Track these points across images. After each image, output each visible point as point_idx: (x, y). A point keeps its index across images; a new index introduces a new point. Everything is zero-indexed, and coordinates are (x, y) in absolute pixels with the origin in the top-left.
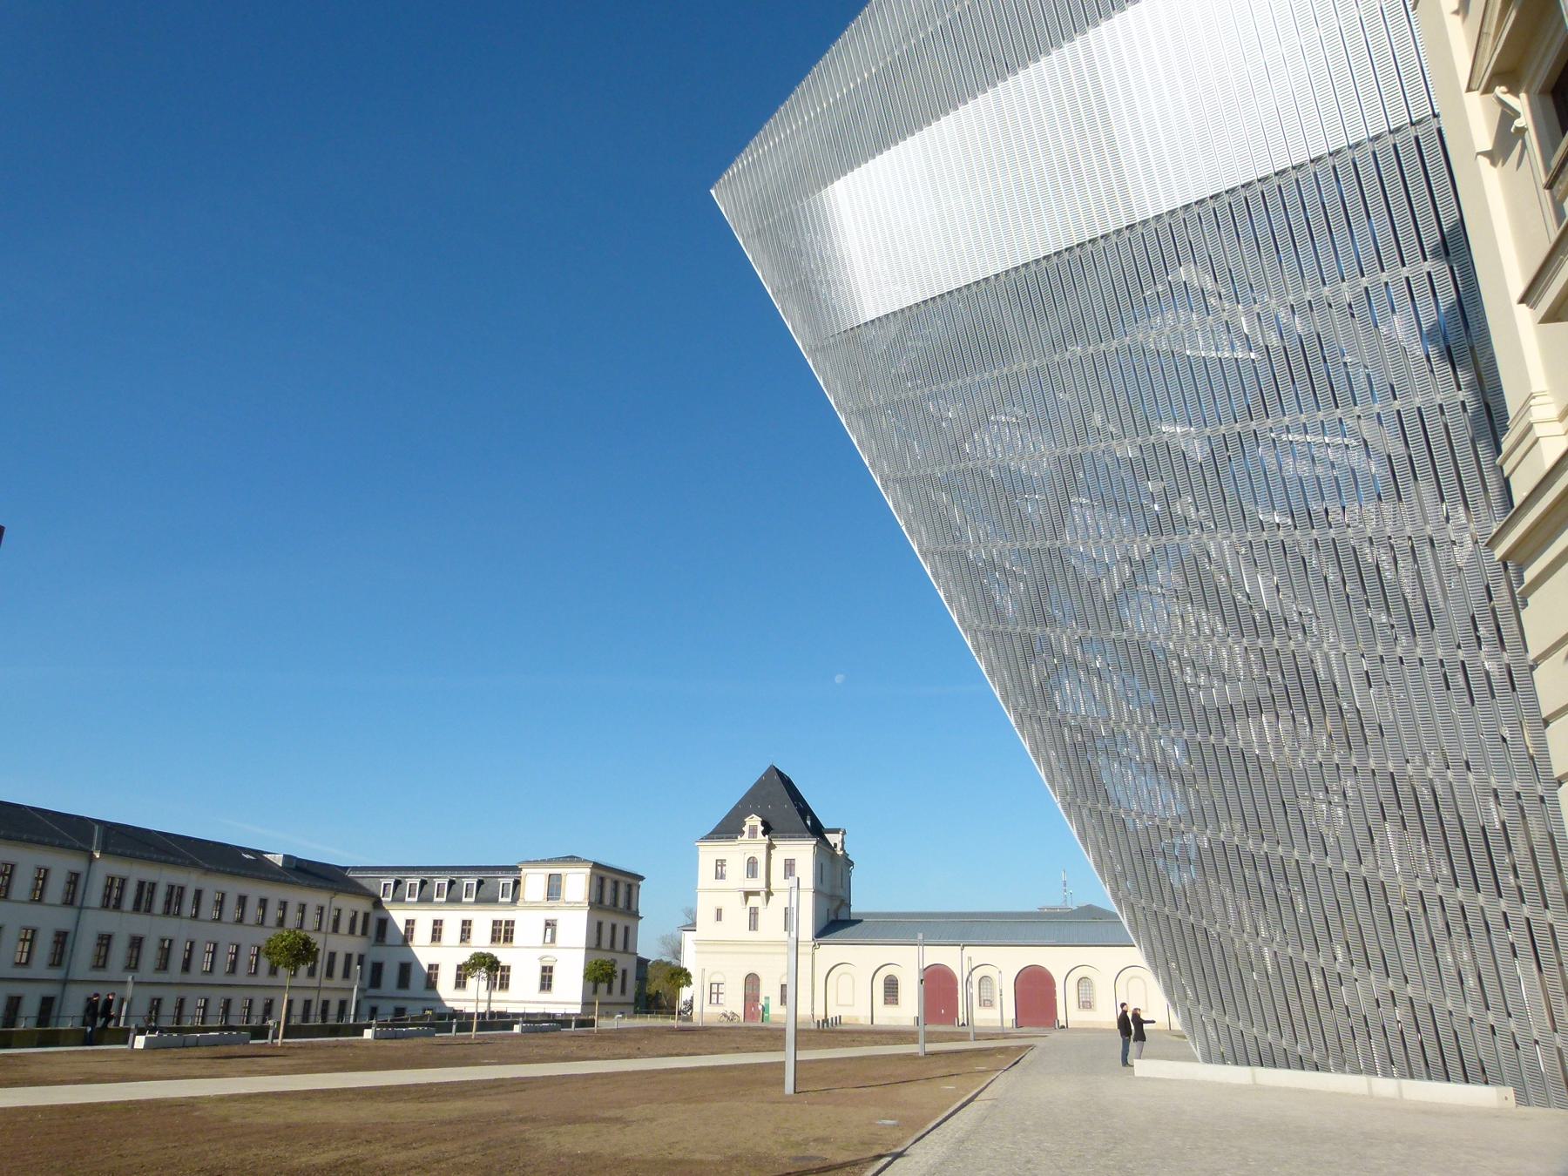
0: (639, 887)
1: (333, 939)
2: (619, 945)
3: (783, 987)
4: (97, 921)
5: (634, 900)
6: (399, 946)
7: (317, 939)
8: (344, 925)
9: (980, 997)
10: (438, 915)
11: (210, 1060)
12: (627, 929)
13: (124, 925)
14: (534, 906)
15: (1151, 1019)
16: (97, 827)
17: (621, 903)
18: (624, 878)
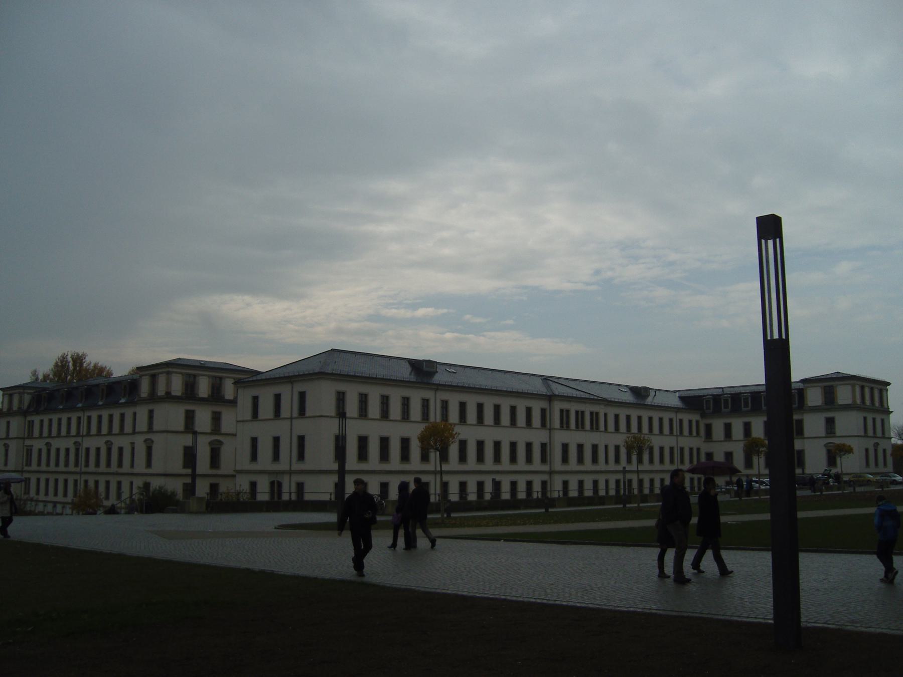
0: (887, 390)
1: (680, 439)
2: (879, 433)
3: (867, 450)
4: (561, 437)
6: (721, 441)
7: (463, 432)
10: (727, 421)
12: (883, 421)
13: (573, 438)
14: (815, 409)
15: (153, 462)
16: (424, 363)
18: (868, 384)
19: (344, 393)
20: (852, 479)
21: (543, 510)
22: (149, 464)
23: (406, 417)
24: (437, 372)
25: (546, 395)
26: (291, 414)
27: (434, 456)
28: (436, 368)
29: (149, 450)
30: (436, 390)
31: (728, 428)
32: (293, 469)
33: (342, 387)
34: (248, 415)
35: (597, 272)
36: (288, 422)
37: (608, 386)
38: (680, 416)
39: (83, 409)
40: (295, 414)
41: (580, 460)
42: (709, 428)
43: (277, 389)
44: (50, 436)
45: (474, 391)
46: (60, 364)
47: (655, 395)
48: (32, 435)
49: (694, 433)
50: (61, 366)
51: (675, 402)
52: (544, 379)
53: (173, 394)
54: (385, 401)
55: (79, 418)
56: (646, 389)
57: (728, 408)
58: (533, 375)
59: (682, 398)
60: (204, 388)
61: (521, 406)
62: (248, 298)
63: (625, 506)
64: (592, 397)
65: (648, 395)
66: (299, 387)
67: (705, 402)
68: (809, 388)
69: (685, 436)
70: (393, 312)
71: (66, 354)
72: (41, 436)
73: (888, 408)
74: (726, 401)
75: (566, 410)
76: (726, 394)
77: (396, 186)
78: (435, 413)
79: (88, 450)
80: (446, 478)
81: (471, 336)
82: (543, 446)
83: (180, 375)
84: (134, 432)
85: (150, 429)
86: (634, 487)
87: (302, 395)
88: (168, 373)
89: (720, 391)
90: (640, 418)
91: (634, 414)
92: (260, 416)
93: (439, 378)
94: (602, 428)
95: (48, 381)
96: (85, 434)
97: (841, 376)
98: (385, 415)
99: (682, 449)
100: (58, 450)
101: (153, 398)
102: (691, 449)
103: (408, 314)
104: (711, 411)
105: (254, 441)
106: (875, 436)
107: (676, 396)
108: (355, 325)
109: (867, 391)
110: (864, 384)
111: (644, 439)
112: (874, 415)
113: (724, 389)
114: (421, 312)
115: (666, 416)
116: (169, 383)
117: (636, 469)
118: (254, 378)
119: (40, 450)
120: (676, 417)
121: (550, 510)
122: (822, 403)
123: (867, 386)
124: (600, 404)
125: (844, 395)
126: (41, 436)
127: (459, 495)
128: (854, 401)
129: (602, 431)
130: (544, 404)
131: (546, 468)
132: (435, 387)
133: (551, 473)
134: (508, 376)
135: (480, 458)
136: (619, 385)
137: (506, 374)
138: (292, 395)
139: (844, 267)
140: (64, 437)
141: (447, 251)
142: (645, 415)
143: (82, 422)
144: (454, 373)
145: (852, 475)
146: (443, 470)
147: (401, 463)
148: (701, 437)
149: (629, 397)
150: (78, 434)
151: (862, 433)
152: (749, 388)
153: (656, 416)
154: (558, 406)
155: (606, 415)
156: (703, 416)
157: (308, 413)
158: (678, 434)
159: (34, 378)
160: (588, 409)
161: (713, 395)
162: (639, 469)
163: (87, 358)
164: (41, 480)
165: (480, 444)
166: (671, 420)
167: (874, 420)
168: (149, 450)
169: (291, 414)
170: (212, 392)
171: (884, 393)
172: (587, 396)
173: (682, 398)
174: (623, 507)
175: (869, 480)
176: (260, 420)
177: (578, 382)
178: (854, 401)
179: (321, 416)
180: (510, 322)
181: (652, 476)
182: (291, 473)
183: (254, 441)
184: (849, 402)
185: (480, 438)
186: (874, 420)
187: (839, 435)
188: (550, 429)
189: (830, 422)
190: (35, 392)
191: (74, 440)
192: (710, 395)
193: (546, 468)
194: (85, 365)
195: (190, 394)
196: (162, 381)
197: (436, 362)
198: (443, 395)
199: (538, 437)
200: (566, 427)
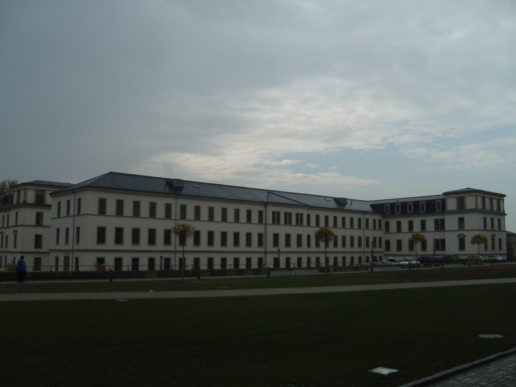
0: (503, 200)
4: (272, 229)
5: (501, 207)
7: (335, 231)
8: (371, 226)
9: (74, 225)
10: (399, 220)
13: (282, 230)
14: (452, 212)
16: (175, 181)
17: (495, 209)
18: (495, 197)
19: (122, 201)
24: (184, 187)
25: (263, 202)
26: (74, 214)
27: (322, 244)
31: (399, 224)
33: (103, 195)
35: (385, 139)
37: (295, 195)
38: (366, 217)
40: (76, 214)
41: (352, 245)
42: (387, 224)
45: (198, 198)
47: (352, 203)
49: (377, 228)
52: (268, 192)
53: (28, 202)
56: (345, 200)
59: (372, 206)
63: (111, 281)
65: (346, 204)
66: (79, 196)
67: (385, 208)
70: (267, 162)
73: (504, 212)
74: (398, 207)
77: (274, 93)
78: (176, 213)
80: (328, 255)
81: (310, 175)
82: (260, 236)
83: (33, 190)
87: (79, 200)
89: (396, 201)
90: (352, 219)
92: (61, 216)
98: (224, 219)
99: (368, 238)
101: (19, 205)
109: (487, 201)
112: (492, 216)
113: (398, 200)
114: (285, 162)
116: (25, 195)
117: (324, 250)
118: (67, 189)
121: (114, 280)
122: (457, 208)
124: (303, 208)
125: (470, 203)
127: (148, 266)
129: (305, 226)
130: (262, 208)
131: (262, 249)
133: (265, 253)
138: (75, 201)
141: (300, 128)
144: (198, 187)
145: (469, 256)
146: (184, 250)
147: (208, 247)
148: (383, 230)
149: (333, 205)
151: (483, 228)
153: (348, 217)
154: (271, 209)
156: (384, 216)
157: (82, 213)
160: (294, 212)
162: (327, 251)
164: (3, 257)
166: (359, 220)
167: (492, 219)
169: (74, 214)
171: (501, 202)
172: (294, 203)
173: (372, 206)
176: (311, 227)
179: (87, 214)
180: (335, 167)
183: (58, 230)
186: (492, 219)
187: (143, 216)
189: (461, 220)
192: (389, 203)
193: (276, 249)
196: (22, 193)
199: (255, 229)
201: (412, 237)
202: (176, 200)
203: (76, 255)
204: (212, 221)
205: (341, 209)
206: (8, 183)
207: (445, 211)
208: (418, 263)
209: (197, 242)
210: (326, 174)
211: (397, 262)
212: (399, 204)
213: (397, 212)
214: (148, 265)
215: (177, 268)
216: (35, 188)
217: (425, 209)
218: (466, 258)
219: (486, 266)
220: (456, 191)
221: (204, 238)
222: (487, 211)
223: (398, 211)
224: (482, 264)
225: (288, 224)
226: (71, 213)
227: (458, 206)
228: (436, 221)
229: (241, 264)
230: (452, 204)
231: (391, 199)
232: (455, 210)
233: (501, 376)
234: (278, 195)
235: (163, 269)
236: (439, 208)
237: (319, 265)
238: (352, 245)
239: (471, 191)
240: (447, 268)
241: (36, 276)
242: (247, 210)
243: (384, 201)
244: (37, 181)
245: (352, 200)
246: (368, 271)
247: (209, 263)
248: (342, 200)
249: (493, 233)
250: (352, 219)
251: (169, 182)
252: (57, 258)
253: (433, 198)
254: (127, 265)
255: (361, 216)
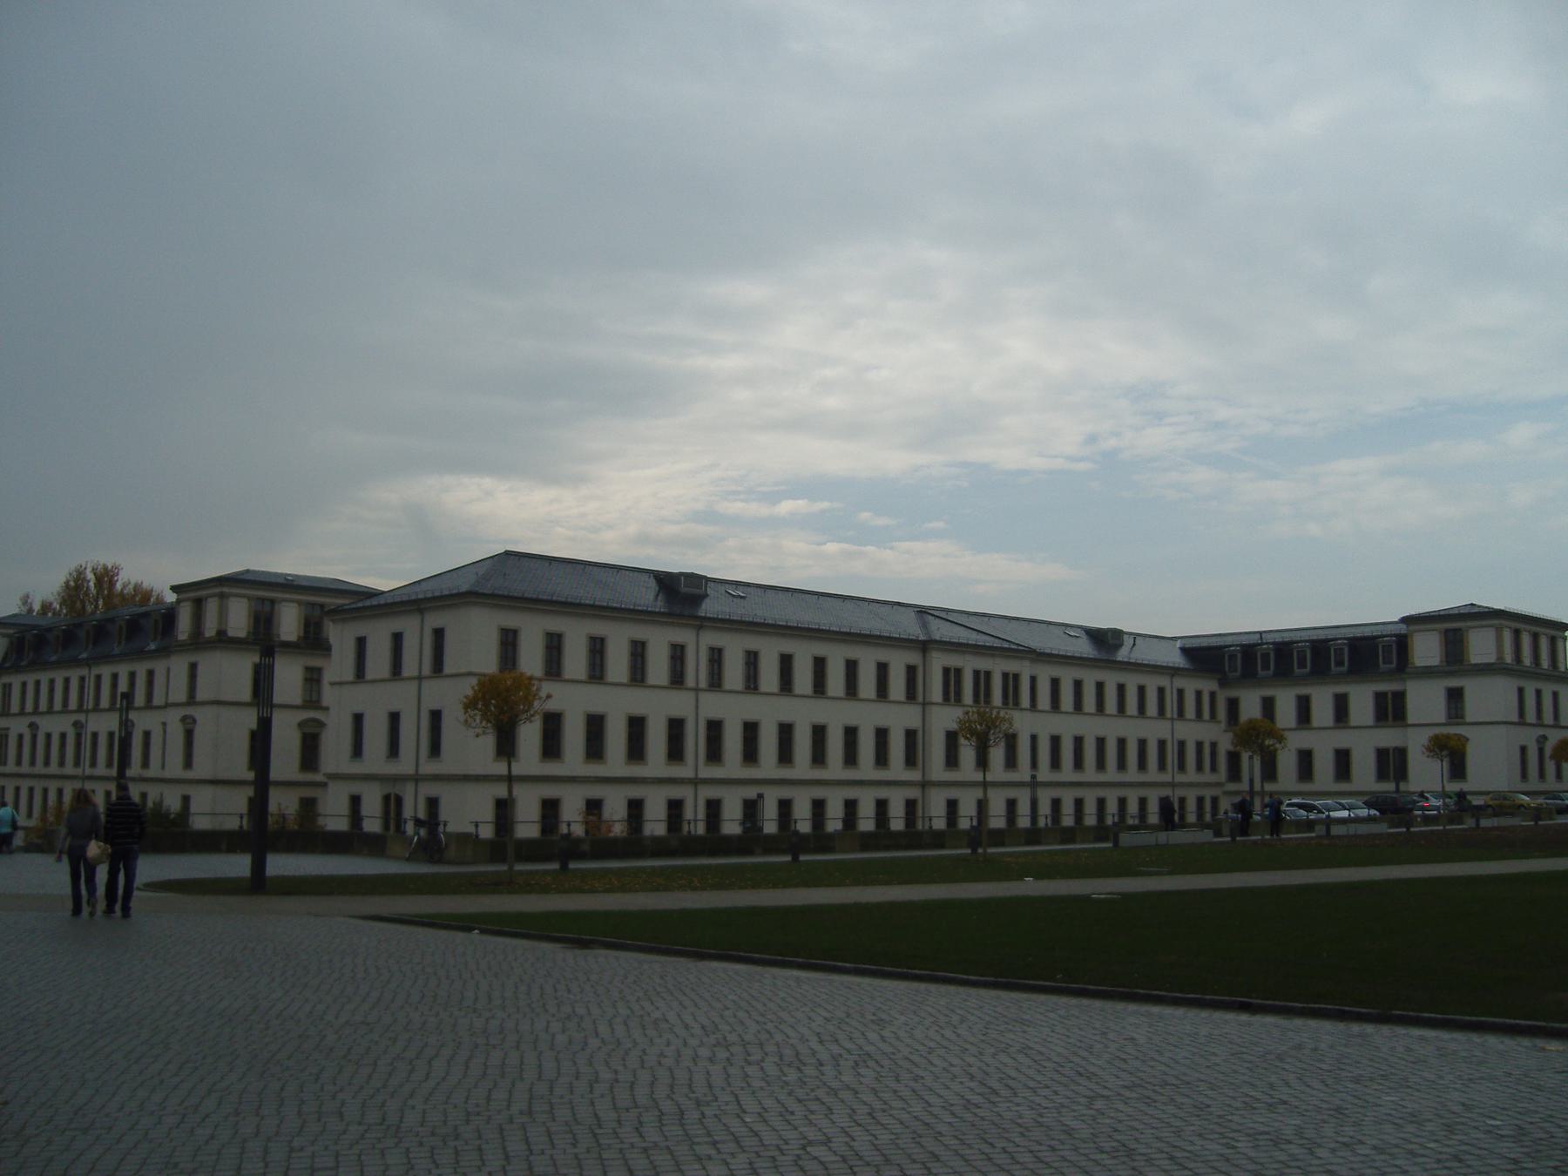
1: (1179, 725)
2: (1548, 718)
3: (1523, 749)
8: (1111, 704)
10: (1268, 692)
11: (361, 922)
14: (1428, 673)
18: (1528, 627)
19: (602, 640)
20: (1491, 803)
21: (788, 858)
22: (188, 763)
23: (639, 677)
26: (420, 672)
28: (706, 587)
29: (189, 735)
30: (700, 628)
32: (421, 771)
33: (511, 620)
34: (349, 674)
35: (1092, 439)
36: (415, 684)
39: (88, 663)
40: (427, 670)
43: (396, 624)
44: (36, 712)
46: (72, 583)
47: (1134, 645)
48: (9, 709)
49: (1206, 715)
50: (74, 590)
51: (1176, 659)
53: (231, 633)
54: (597, 648)
55: (82, 679)
56: (1117, 634)
57: (1269, 669)
58: (899, 604)
59: (1187, 652)
60: (289, 624)
61: (868, 660)
62: (488, 482)
63: (795, 859)
64: (1006, 645)
65: (1121, 645)
66: (434, 620)
67: (1227, 658)
68: (1416, 634)
69: (1205, 721)
70: (736, 507)
71: (84, 566)
72: (22, 713)
74: (1265, 656)
75: (955, 669)
76: (1267, 643)
77: (748, 291)
79: (95, 735)
81: (870, 548)
82: (910, 735)
83: (296, 605)
84: (167, 706)
85: (191, 700)
86: (797, 818)
87: (439, 634)
88: (222, 596)
90: (1078, 685)
91: (1090, 678)
92: (369, 675)
93: (709, 608)
94: (1025, 700)
95: (50, 614)
96: (90, 707)
97: (1476, 610)
99: (1182, 744)
100: (49, 736)
101: (198, 642)
102: (1199, 745)
103: (763, 510)
104: (1238, 674)
105: (358, 719)
106: (1540, 723)
107: (1175, 645)
108: (670, 530)
109: (1526, 640)
110: (1538, 629)
111: (997, 717)
112: (1540, 685)
113: (1264, 636)
114: (785, 507)
115: (1152, 683)
116: (223, 614)
118: (368, 603)
119: (21, 737)
120: (1171, 685)
121: (802, 858)
122: (1441, 662)
123: (1544, 634)
124: (1022, 658)
125: (1481, 646)
126: (65, 709)
127: (666, 823)
128: (1500, 657)
130: (913, 658)
131: (914, 775)
132: (698, 623)
133: (925, 785)
134: (848, 604)
135: (851, 758)
136: (1067, 625)
137: (846, 601)
139: (1521, 434)
140: (15, 715)
141: (831, 402)
142: (1111, 680)
143: (86, 685)
144: (742, 597)
145: (1491, 795)
147: (812, 768)
149: (1084, 648)
150: (80, 709)
151: (1515, 718)
152: (1309, 633)
153: (1132, 682)
154: (939, 662)
155: (1033, 680)
156: (1224, 683)
157: (448, 668)
158: (1175, 716)
159: (24, 610)
161: (1242, 646)
163: (120, 577)
165: (851, 734)
166: (1161, 691)
167: (1538, 693)
168: (189, 735)
169: (420, 672)
170: (306, 632)
171: (1560, 644)
172: (997, 643)
173: (1187, 652)
174: (972, 853)
175: (1522, 806)
176: (1108, 715)
177: (986, 619)
178: (1500, 657)
180: (940, 525)
181: (1143, 792)
182: (417, 779)
183: (358, 719)
184: (1492, 659)
185: (751, 717)
186: (1538, 693)
188: (924, 704)
189: (1455, 696)
190: (15, 633)
191: (75, 717)
193: (914, 775)
194: (119, 586)
195: (263, 639)
196: (211, 608)
197: (705, 577)
198: (710, 638)
199: (899, 718)
200: (955, 700)
201: (1430, 741)
202: (698, 635)
203: (428, 790)
204: (754, 693)
205: (1108, 661)
206: (95, 574)
207: (1408, 670)
208: (1375, 815)
209: (551, 746)
210: (917, 546)
211: (1320, 812)
212: (1268, 649)
213: (1262, 670)
214: (625, 821)
215: (701, 829)
216: (300, 597)
217: (1346, 663)
218: (1482, 803)
219: (1562, 824)
220: (1451, 612)
221: (574, 737)
222: (1526, 669)
223: (1266, 667)
224: (1551, 819)
225: (953, 700)
226: (409, 668)
227: (1447, 656)
228: (1380, 698)
229: (378, 820)
230: (1427, 650)
231: (1241, 633)
232: (1436, 666)
233: (1449, 1157)
234: (944, 619)
235: (1050, 825)
236: (1387, 661)
237: (680, 829)
238: (1078, 764)
239: (1479, 613)
240: (1339, 837)
241: (603, 847)
242: (815, 658)
243: (1219, 639)
244: (248, 571)
245: (1136, 636)
246: (1313, 835)
247: (544, 817)
248: (1110, 634)
249: (1542, 733)
250: (1055, 683)
251: (668, 583)
252: (355, 801)
253: (1367, 632)
254: (695, 821)
255: (1164, 681)
